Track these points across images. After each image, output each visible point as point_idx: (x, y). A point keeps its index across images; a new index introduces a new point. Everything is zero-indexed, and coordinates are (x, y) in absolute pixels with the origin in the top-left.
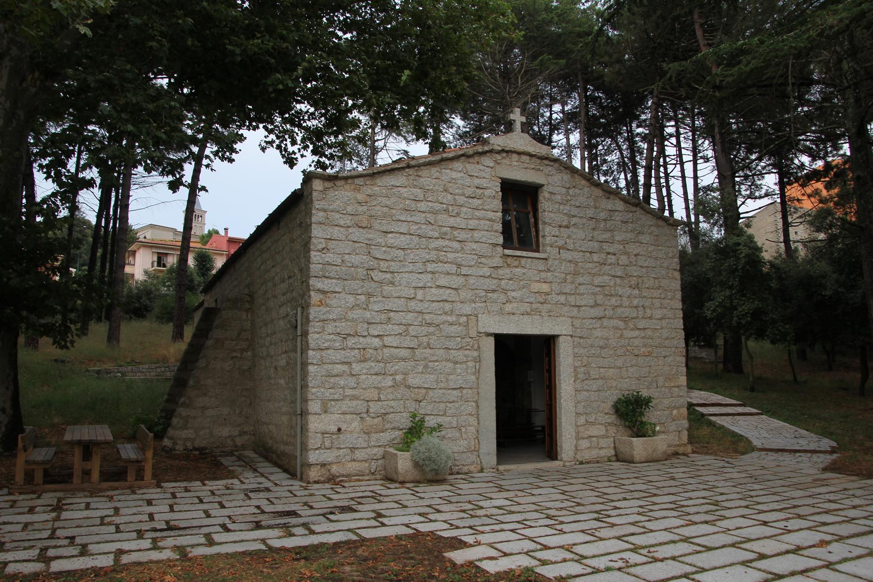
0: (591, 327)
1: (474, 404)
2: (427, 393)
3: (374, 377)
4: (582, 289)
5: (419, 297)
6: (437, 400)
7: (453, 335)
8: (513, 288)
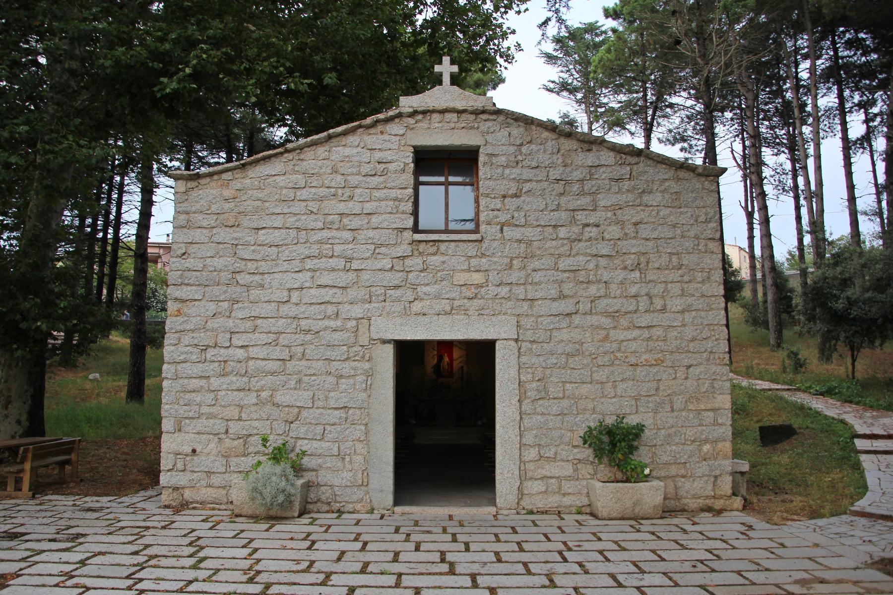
0: (552, 327)
1: (363, 428)
2: (299, 413)
3: (235, 393)
4: (537, 277)
5: (294, 299)
6: (313, 421)
7: (336, 343)
8: (426, 282)
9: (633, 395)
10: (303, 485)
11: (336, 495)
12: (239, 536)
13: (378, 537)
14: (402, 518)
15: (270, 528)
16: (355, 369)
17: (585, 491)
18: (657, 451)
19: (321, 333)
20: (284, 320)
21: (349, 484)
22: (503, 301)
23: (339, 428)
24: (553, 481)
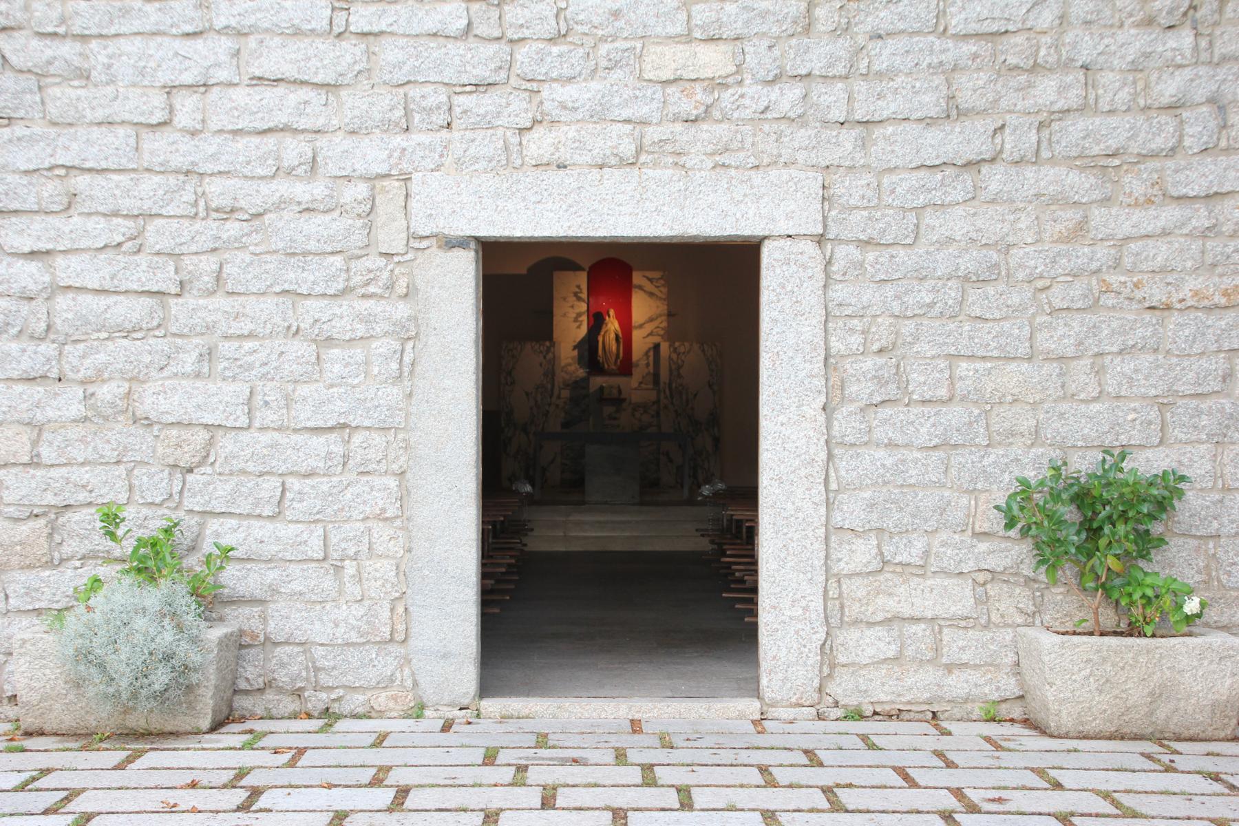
0: (921, 201)
1: (392, 483)
2: (211, 442)
3: (19, 388)
4: (884, 55)
5: (183, 118)
6: (251, 467)
7: (312, 246)
8: (567, 71)
9: (1153, 392)
10: (224, 643)
11: (317, 670)
12: (37, 784)
13: (439, 775)
14: (502, 728)
15: (129, 760)
16: (368, 319)
17: (1010, 659)
18: (1220, 553)
19: (267, 218)
20: (157, 179)
21: (354, 637)
22: (783, 126)
23: (324, 485)
24: (919, 628)
